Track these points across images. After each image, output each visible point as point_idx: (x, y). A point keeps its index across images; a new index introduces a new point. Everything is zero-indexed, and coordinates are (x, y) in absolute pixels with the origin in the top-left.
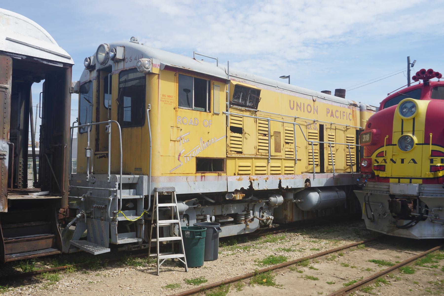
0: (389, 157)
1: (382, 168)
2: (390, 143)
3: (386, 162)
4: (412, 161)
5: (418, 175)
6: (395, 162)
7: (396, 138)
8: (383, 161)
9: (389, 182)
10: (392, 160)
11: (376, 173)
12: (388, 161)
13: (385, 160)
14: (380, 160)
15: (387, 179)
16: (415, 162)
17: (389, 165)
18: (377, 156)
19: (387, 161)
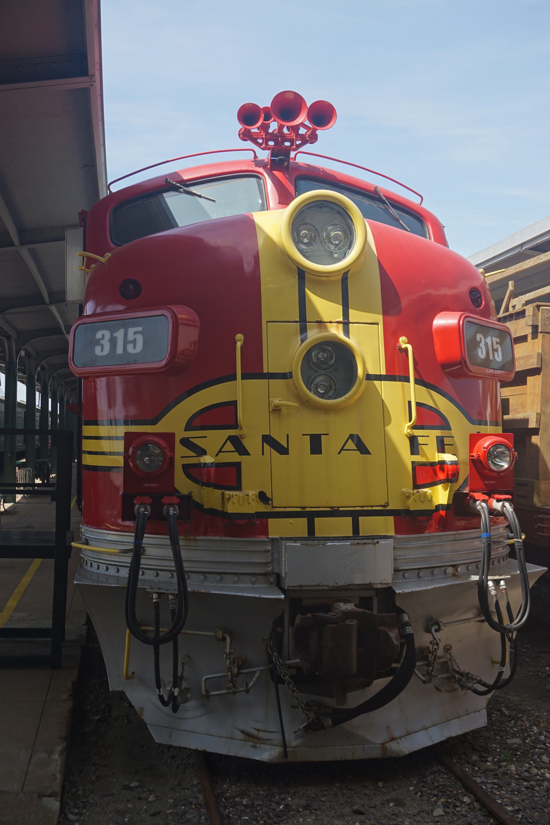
0: (253, 424)
1: (229, 476)
2: (254, 370)
3: (242, 451)
4: (351, 445)
5: (377, 500)
6: (283, 450)
7: (283, 349)
8: (229, 446)
9: (265, 532)
10: (268, 439)
11: (210, 498)
12: (253, 443)
13: (238, 444)
14: (213, 441)
15: (250, 526)
16: (362, 449)
17: (259, 471)
18: (189, 427)
19: (246, 443)
